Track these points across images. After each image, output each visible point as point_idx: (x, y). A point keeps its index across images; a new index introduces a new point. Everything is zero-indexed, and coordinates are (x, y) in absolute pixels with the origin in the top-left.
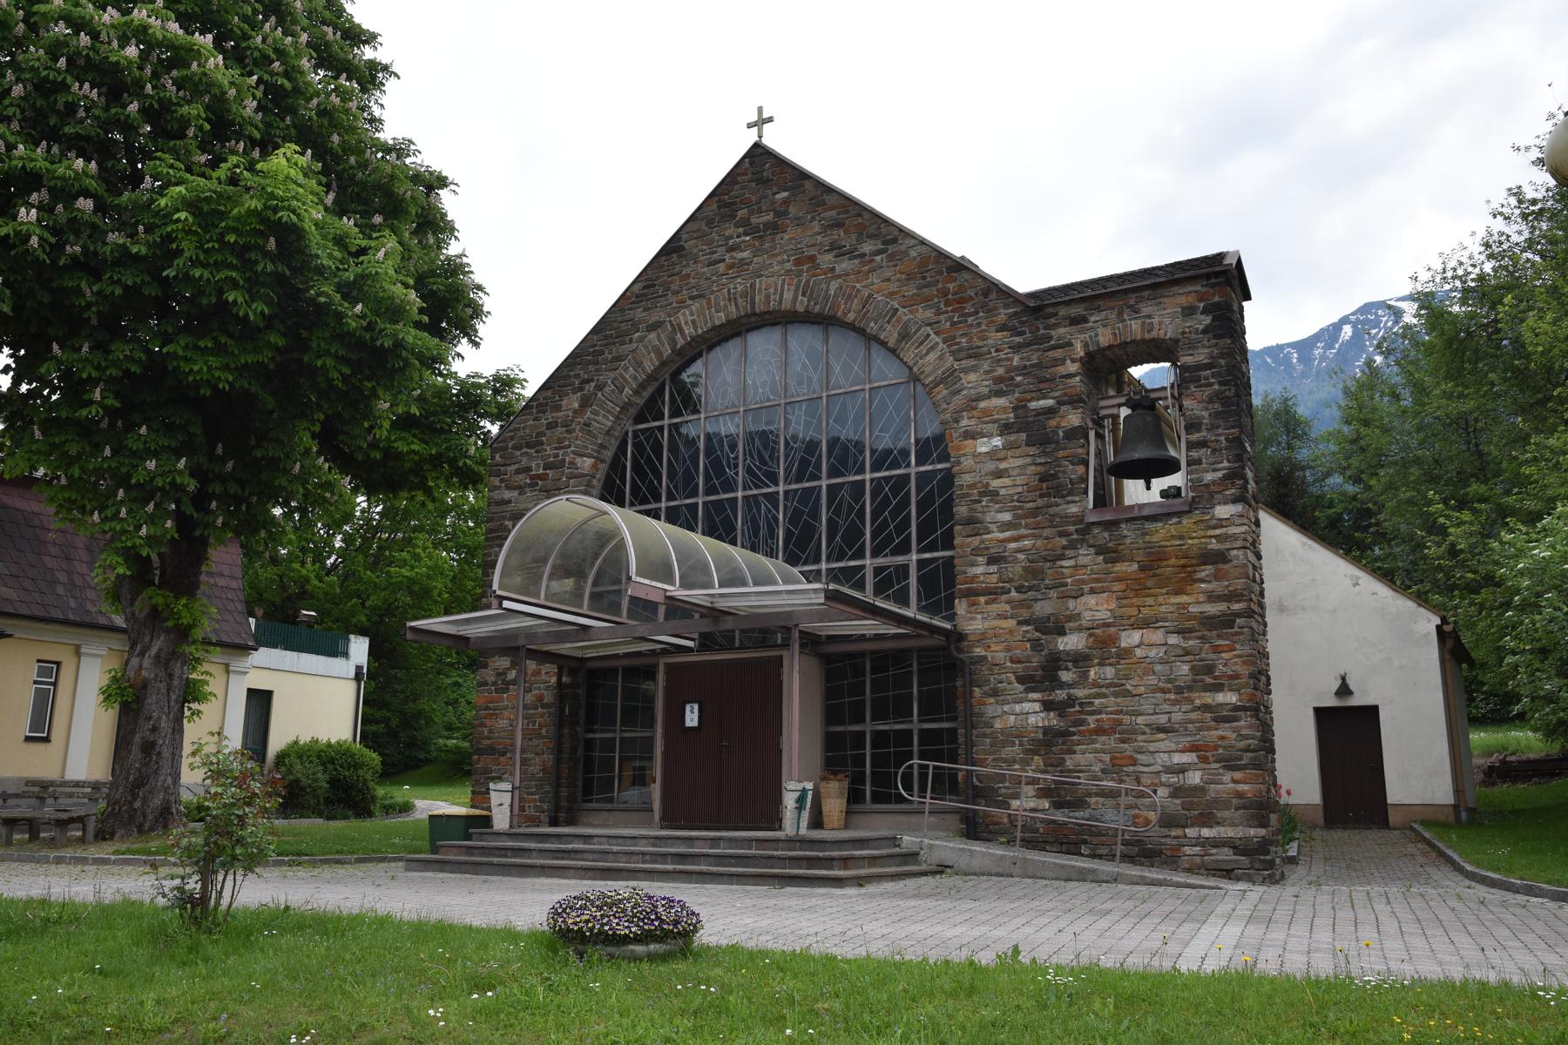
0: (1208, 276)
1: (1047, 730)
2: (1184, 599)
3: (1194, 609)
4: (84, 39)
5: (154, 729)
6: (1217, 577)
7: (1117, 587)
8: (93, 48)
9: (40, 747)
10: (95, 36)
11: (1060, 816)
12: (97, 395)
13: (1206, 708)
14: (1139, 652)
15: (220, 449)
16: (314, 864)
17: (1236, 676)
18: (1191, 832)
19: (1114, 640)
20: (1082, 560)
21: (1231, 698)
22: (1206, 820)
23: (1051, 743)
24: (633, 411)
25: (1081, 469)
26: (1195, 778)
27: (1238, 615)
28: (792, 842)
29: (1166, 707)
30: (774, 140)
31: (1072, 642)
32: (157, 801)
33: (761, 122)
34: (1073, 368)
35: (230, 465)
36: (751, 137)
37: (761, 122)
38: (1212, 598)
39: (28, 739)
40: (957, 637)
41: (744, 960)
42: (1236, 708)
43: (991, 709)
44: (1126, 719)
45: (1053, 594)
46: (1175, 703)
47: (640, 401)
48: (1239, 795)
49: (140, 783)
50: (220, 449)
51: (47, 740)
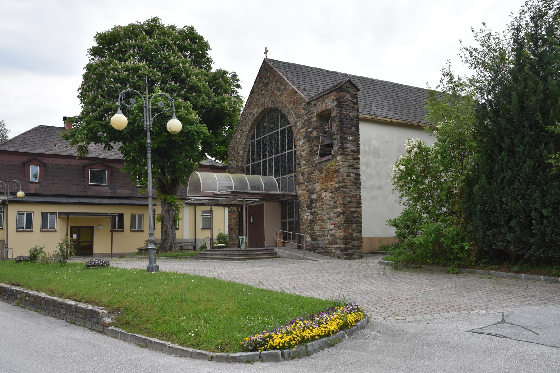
0: (336, 89)
1: (311, 220)
2: (332, 183)
3: (334, 186)
4: (116, 73)
5: (167, 228)
6: (338, 176)
7: (321, 180)
8: (118, 75)
9: (142, 233)
10: (118, 72)
11: (313, 242)
12: (131, 154)
13: (335, 213)
14: (325, 198)
15: (166, 160)
16: (184, 258)
17: (340, 204)
18: (333, 246)
19: (321, 195)
20: (316, 173)
21: (339, 210)
22: (336, 243)
23: (312, 223)
24: (250, 137)
25: (316, 148)
26: (334, 232)
27: (341, 187)
28: (243, 250)
29: (329, 213)
30: (270, 56)
31: (314, 196)
32: (169, 244)
33: (266, 52)
34: (314, 119)
35: (169, 163)
36: (264, 57)
37: (266, 52)
38: (337, 182)
39: (131, 231)
40: (296, 196)
41: (167, 275)
42: (340, 213)
43: (302, 215)
44: (323, 216)
45: (311, 183)
46: (330, 212)
47: (251, 134)
48: (341, 236)
49: (165, 240)
50: (166, 160)
51: (143, 231)
